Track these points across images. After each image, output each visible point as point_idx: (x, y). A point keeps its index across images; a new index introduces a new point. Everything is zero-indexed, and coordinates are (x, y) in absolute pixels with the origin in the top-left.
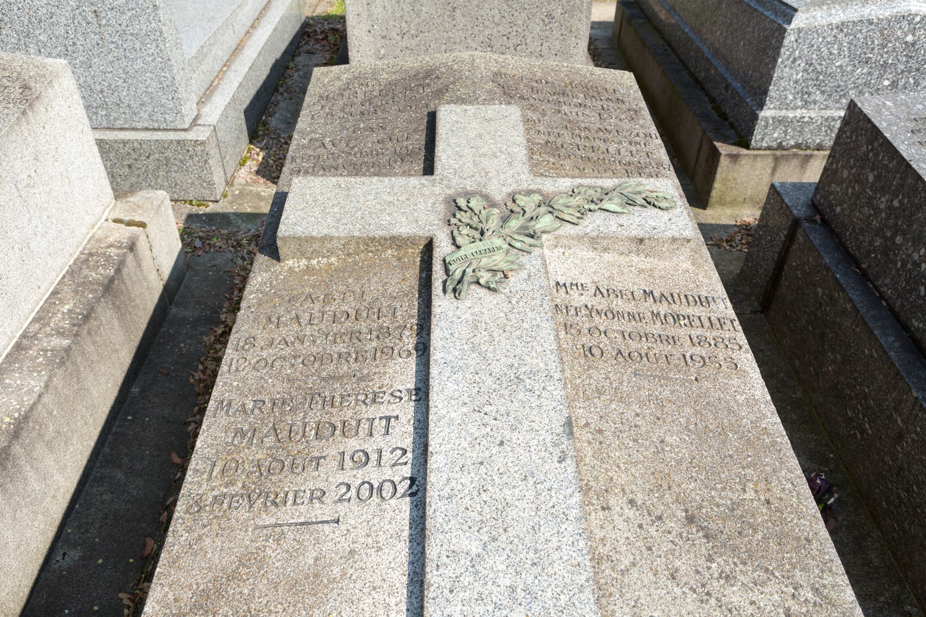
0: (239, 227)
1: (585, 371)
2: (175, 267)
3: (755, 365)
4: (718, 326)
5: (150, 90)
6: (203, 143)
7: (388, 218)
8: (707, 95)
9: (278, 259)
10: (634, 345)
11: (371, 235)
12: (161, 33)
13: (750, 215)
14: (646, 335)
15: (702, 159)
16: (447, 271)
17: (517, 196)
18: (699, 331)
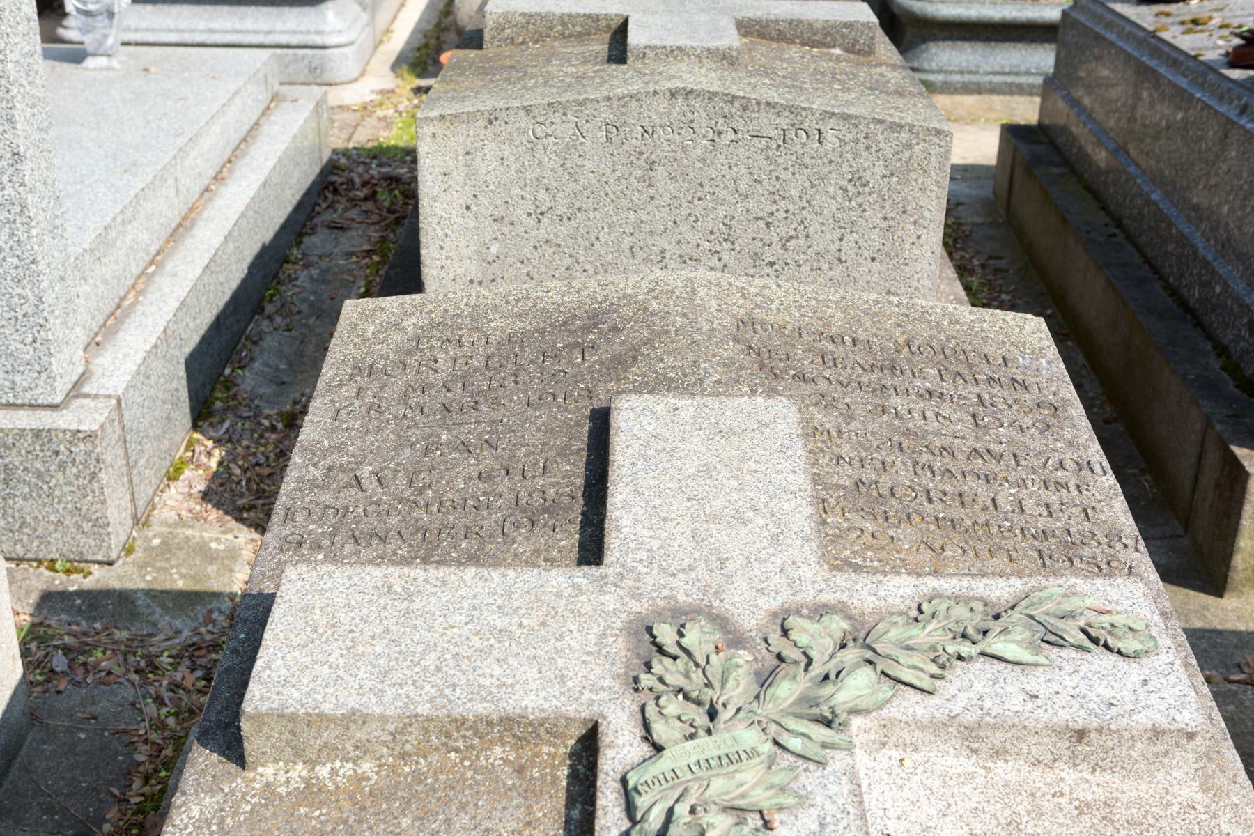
0: (155, 625)
6: (90, 436)
7: (497, 671)
8: (1209, 337)
9: (240, 760)
11: (457, 712)
12: (23, 207)
15: (1208, 480)
16: (630, 809)
17: (792, 621)
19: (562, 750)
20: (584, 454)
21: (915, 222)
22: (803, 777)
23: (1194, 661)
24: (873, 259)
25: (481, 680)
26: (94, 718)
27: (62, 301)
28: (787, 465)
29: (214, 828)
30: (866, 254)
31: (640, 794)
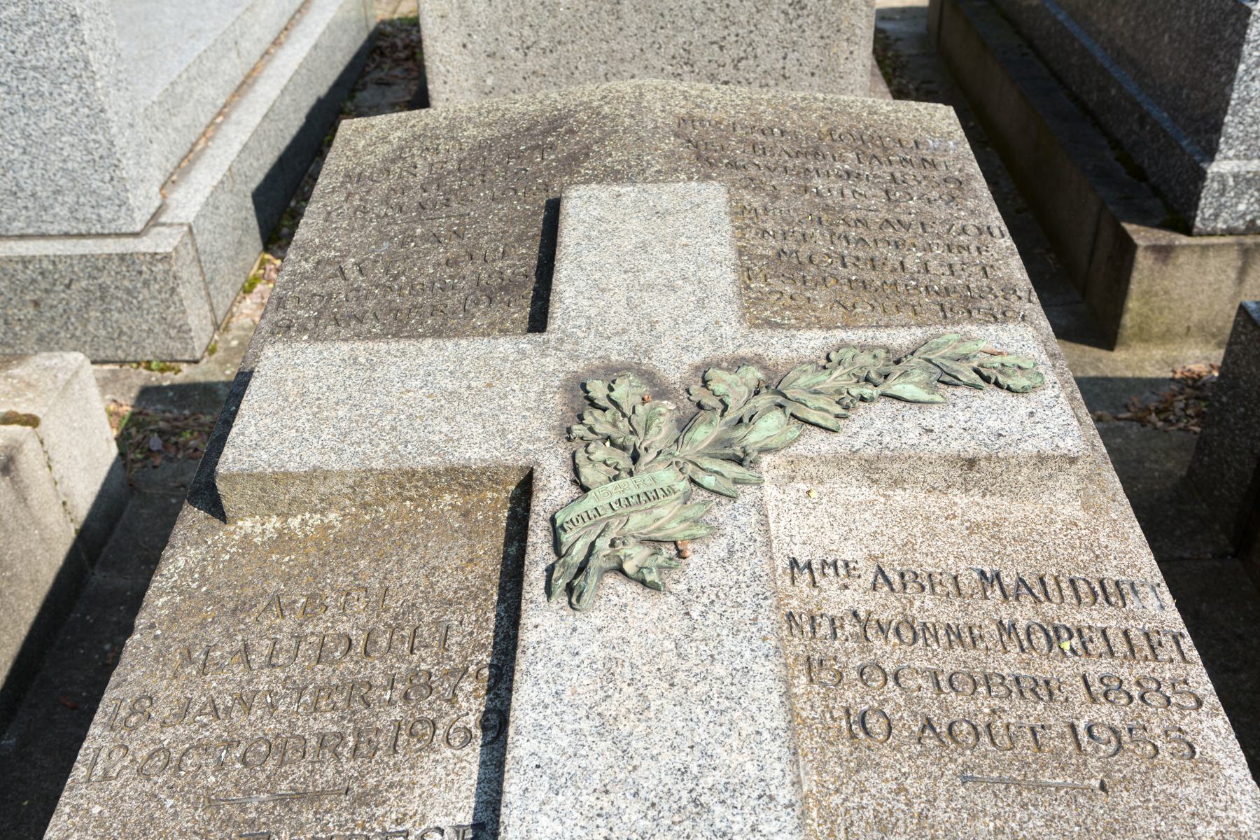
1: (851, 773)
2: (104, 495)
3: (1235, 746)
4: (1147, 651)
5: (70, 165)
6: (166, 258)
10: (960, 704)
11: (407, 466)
12: (87, 63)
13: (1201, 359)
14: (987, 678)
16: (557, 544)
17: (712, 373)
18: (1105, 666)
19: (504, 495)
20: (539, 239)
21: (848, 39)
22: (715, 511)
23: (1079, 396)
24: (813, 74)
25: (431, 437)
26: (183, 486)
27: (133, 145)
28: (715, 239)
29: (196, 576)
30: (807, 70)
31: (565, 531)
